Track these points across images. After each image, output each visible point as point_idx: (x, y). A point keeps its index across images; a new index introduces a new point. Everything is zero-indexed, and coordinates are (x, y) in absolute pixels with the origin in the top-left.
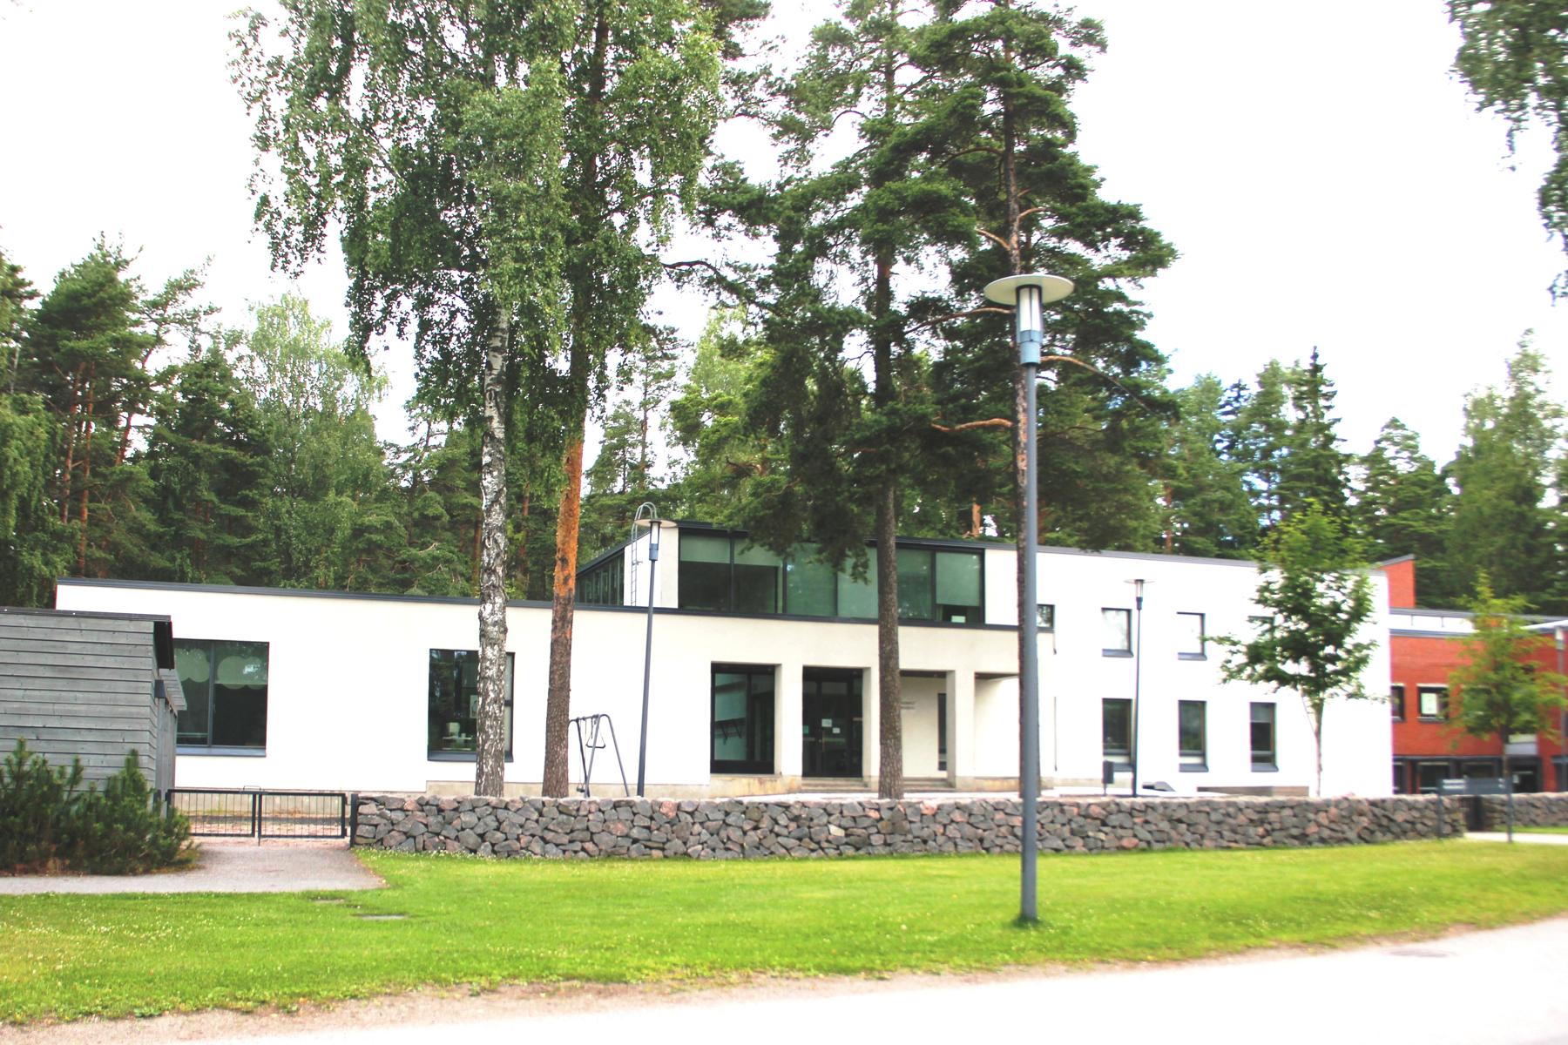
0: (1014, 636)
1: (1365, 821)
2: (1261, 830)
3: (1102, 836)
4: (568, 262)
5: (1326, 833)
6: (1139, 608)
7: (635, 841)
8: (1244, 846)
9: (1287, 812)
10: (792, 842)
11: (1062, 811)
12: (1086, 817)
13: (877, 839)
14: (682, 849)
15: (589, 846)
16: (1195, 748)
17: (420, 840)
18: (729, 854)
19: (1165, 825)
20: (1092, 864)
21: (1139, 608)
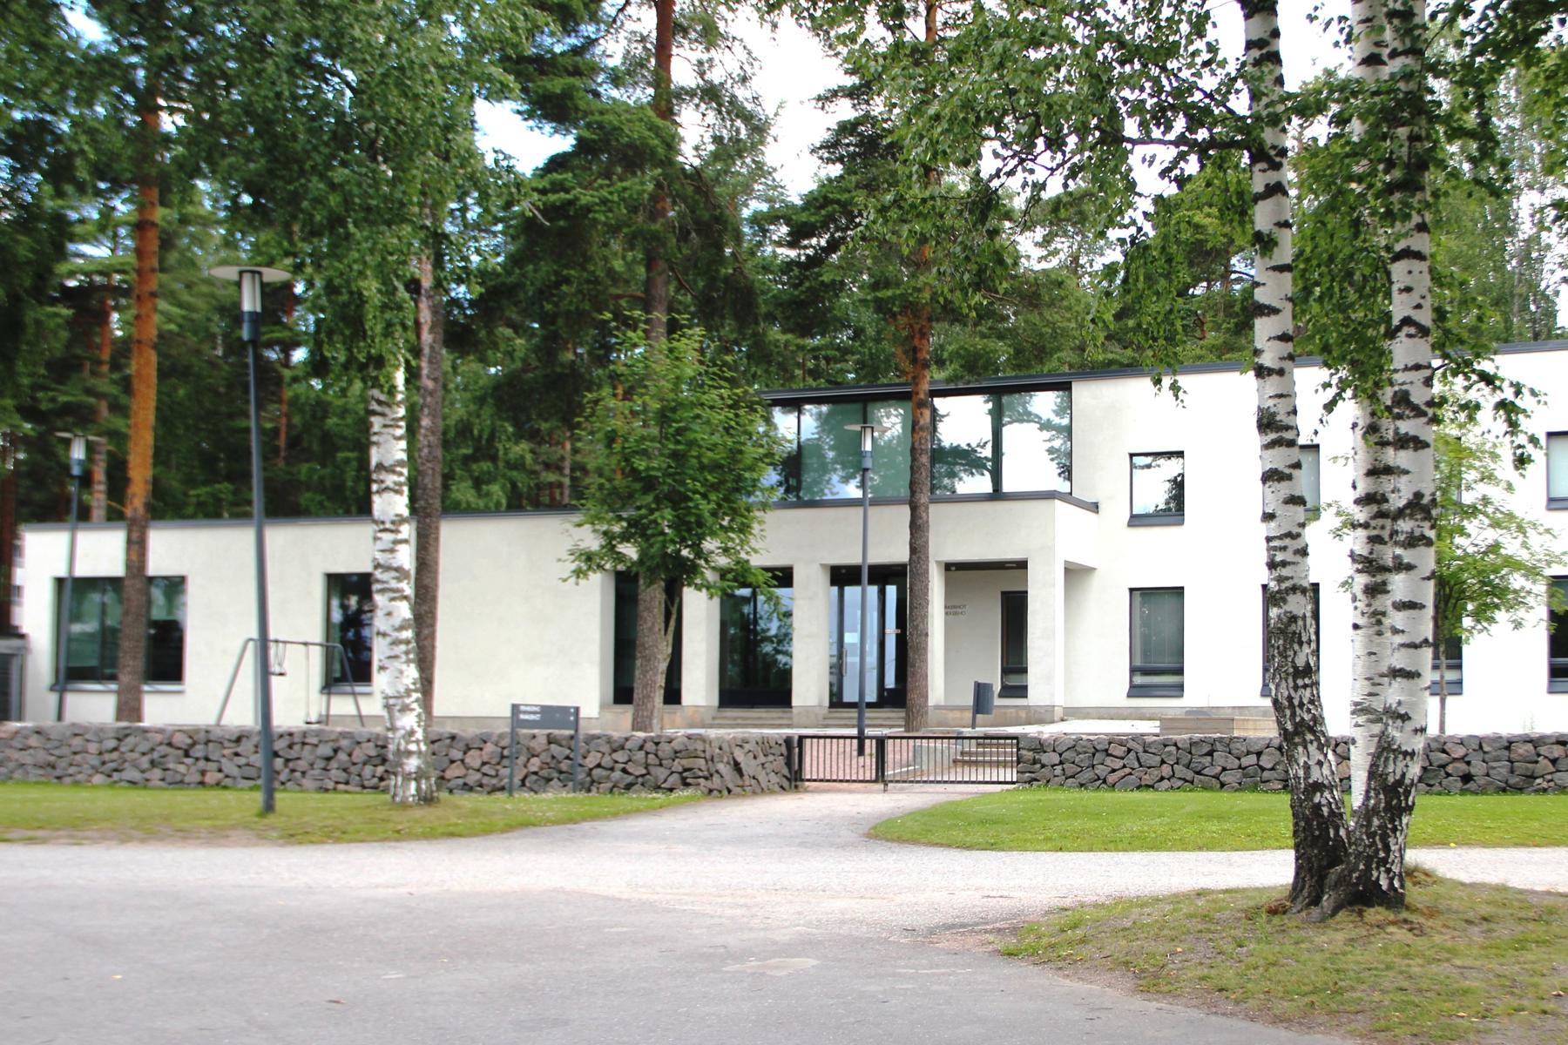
3: (182, 769)
8: (358, 789)
12: (170, 744)
20: (1460, 855)
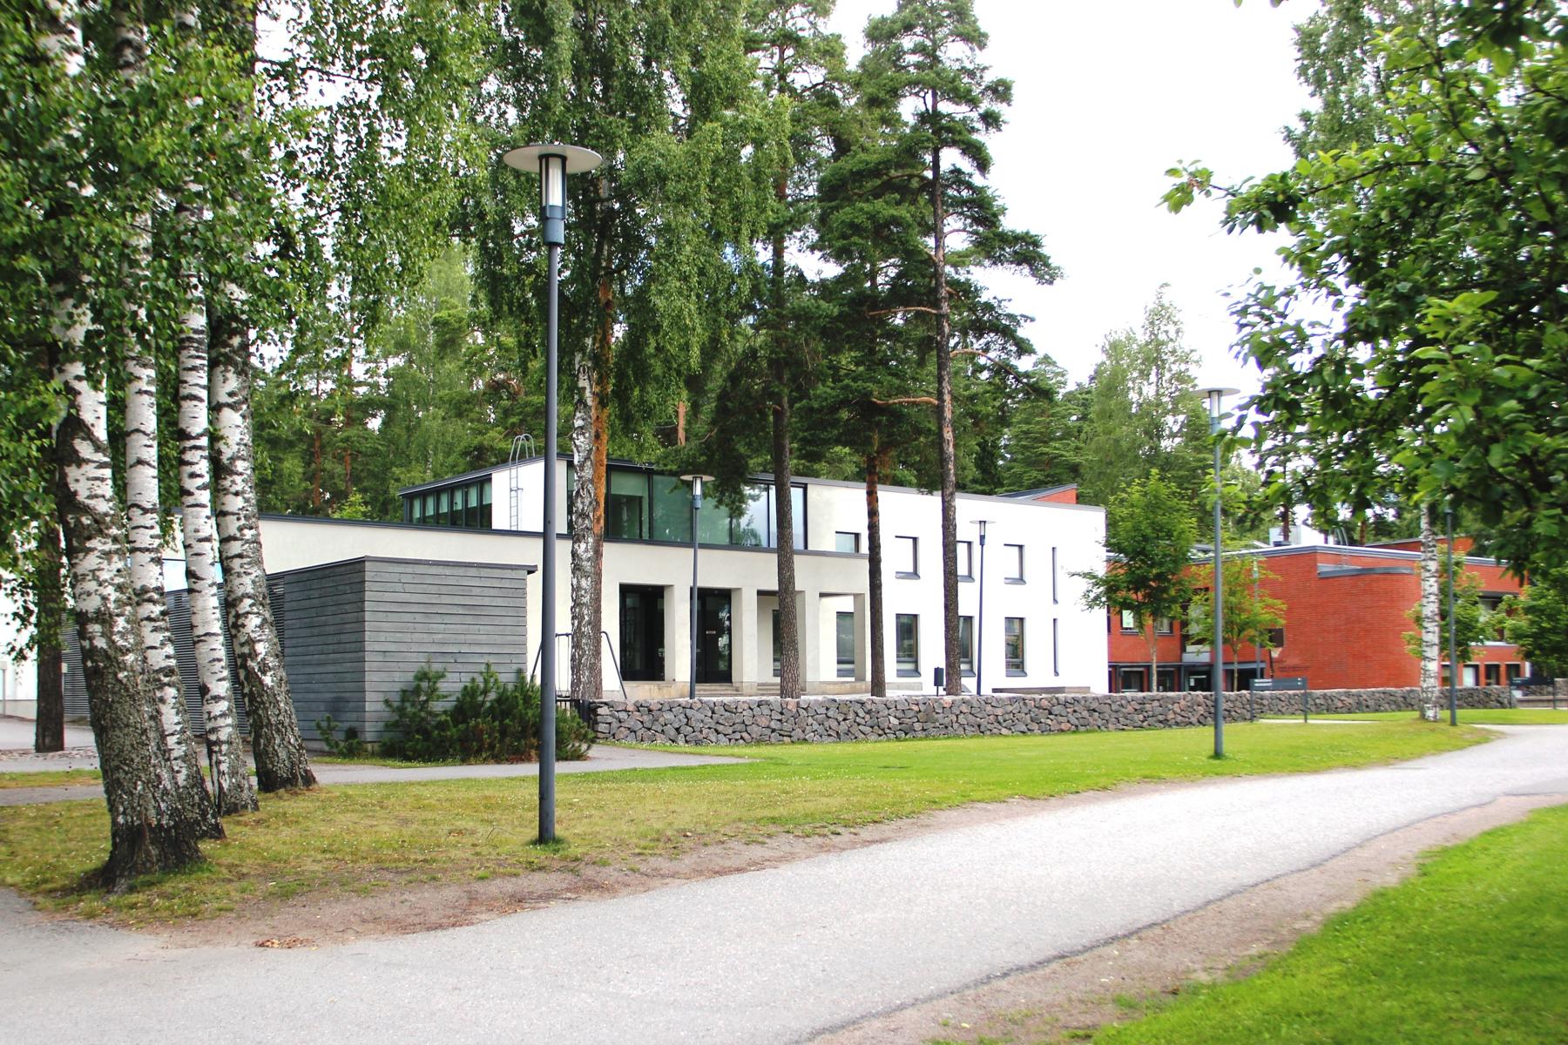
0: (540, 542)
1: (1201, 710)
2: (1141, 717)
3: (1049, 722)
4: (640, 240)
5: (1179, 719)
6: (982, 544)
7: (773, 731)
9: (1156, 704)
10: (868, 729)
11: (1025, 704)
13: (917, 726)
14: (802, 736)
15: (745, 735)
16: (910, 656)
17: (639, 733)
18: (831, 739)
19: (1085, 714)
21: (982, 544)
